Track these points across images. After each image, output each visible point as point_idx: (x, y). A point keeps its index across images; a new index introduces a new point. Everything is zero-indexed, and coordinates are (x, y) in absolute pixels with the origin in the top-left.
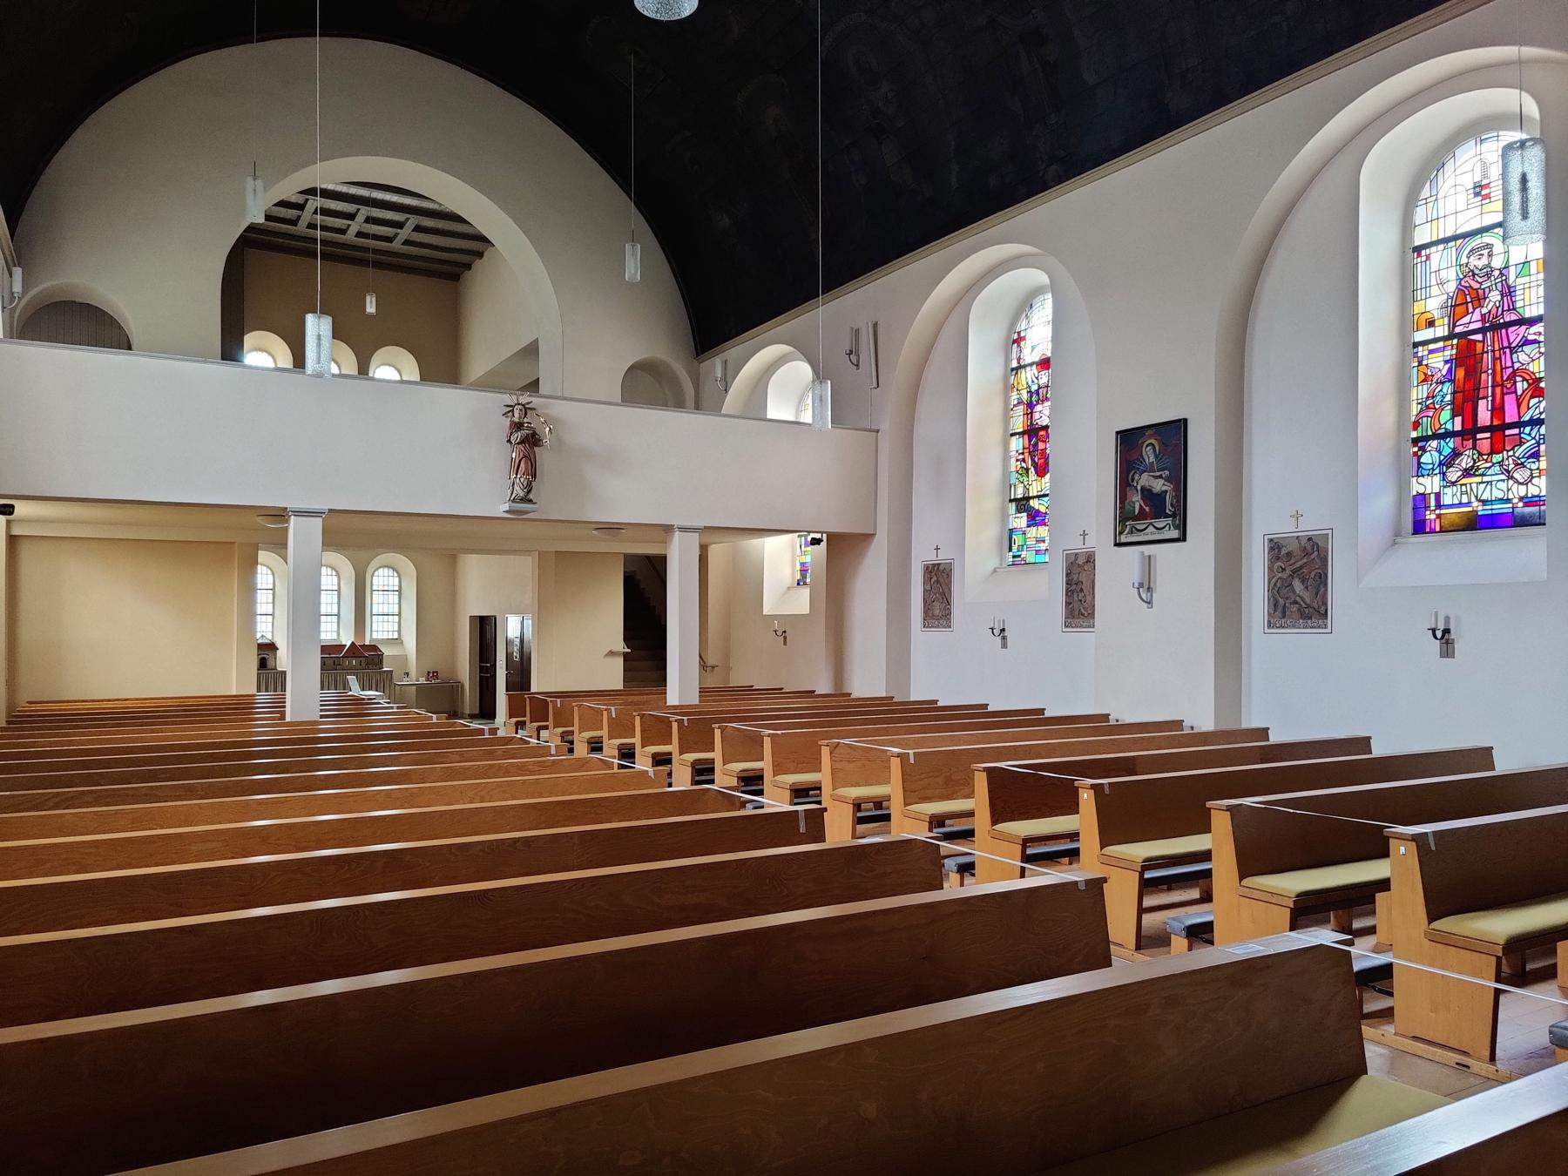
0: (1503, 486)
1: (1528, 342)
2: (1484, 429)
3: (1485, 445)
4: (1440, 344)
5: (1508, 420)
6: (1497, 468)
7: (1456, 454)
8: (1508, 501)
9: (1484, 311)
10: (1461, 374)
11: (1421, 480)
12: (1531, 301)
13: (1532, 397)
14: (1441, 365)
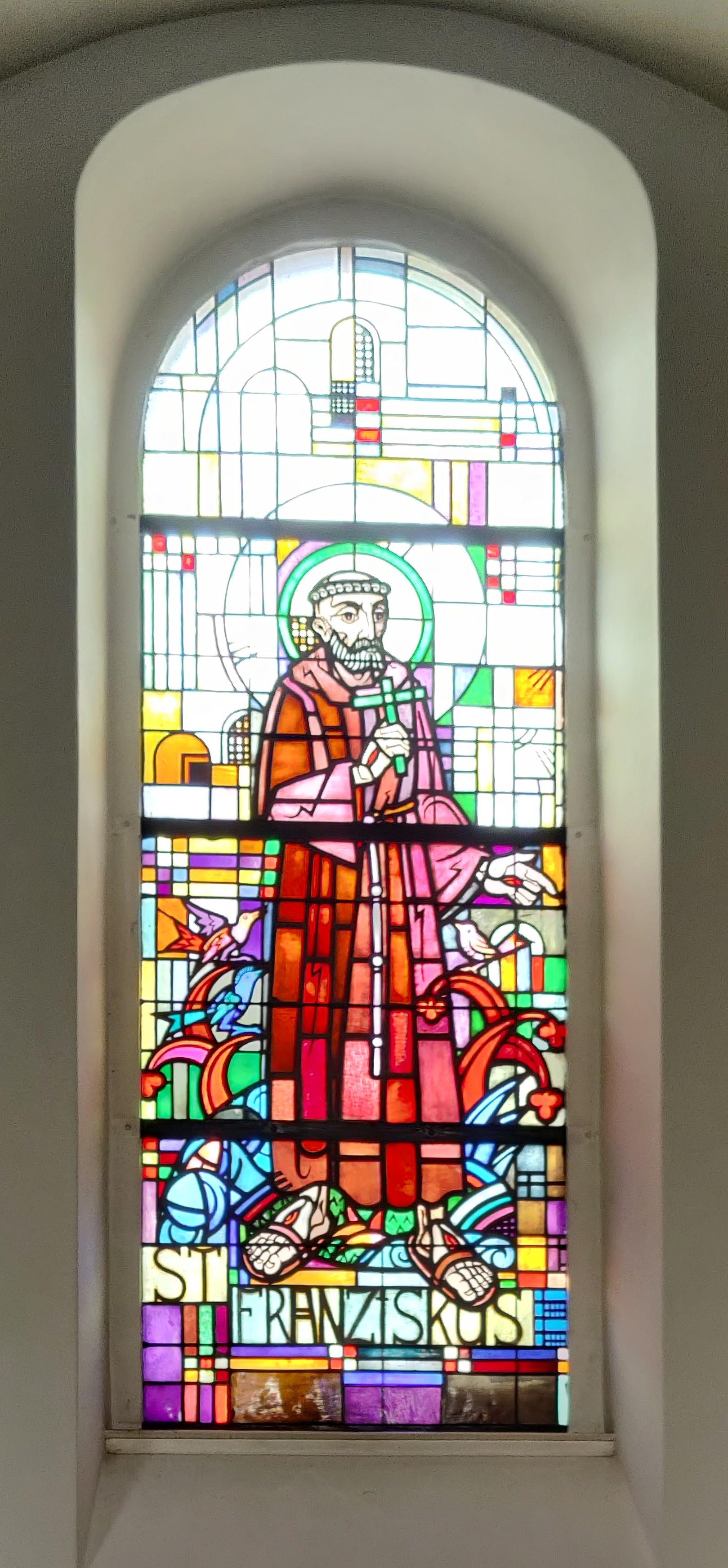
0: (414, 1304)
1: (484, 900)
2: (362, 1131)
3: (362, 1180)
4: (227, 845)
5: (430, 1114)
6: (397, 1254)
7: (277, 1191)
8: (435, 1351)
9: (362, 775)
10: (292, 946)
11: (167, 1257)
12: (508, 774)
13: (496, 1060)
14: (230, 910)
